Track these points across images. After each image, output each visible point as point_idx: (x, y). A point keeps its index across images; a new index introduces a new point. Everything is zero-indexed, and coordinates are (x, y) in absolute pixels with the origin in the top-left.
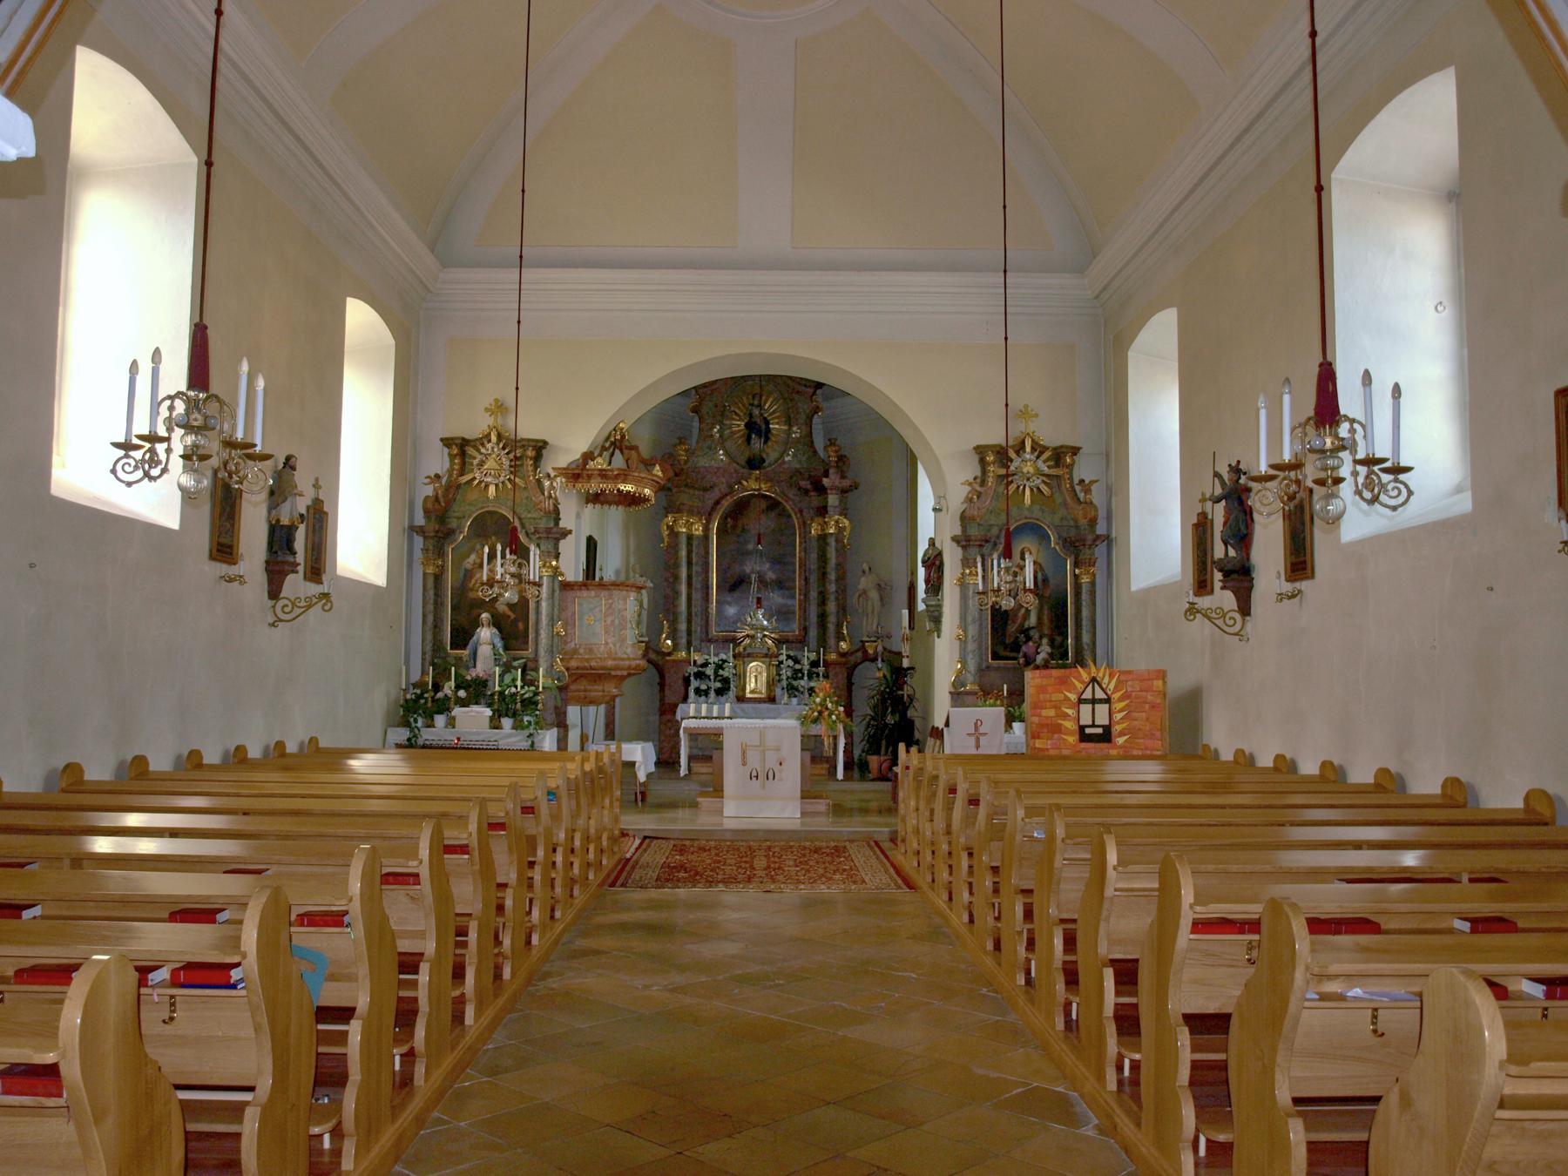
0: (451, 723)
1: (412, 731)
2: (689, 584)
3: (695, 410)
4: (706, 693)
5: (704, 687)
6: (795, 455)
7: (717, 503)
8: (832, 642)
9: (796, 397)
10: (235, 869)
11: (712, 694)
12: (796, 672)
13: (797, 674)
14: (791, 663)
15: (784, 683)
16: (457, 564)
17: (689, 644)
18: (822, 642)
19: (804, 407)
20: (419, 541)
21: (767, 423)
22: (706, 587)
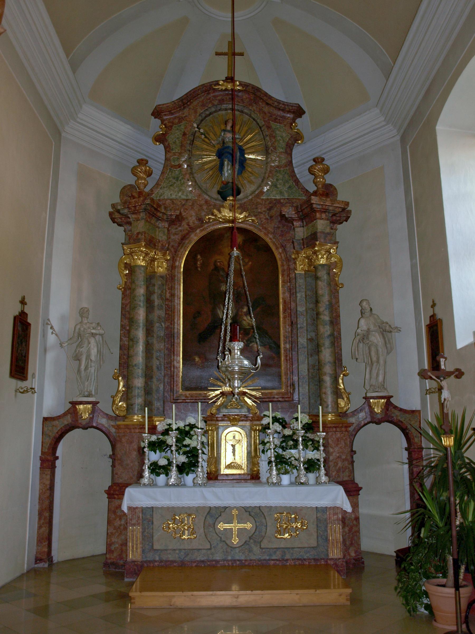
2: (149, 331)
3: (160, 139)
4: (166, 470)
5: (163, 462)
6: (274, 185)
7: (184, 238)
8: (329, 399)
9: (273, 125)
11: (174, 472)
12: (286, 438)
13: (289, 441)
14: (277, 427)
15: (271, 454)
17: (148, 403)
18: (317, 397)
19: (282, 134)
21: (242, 152)
22: (170, 336)
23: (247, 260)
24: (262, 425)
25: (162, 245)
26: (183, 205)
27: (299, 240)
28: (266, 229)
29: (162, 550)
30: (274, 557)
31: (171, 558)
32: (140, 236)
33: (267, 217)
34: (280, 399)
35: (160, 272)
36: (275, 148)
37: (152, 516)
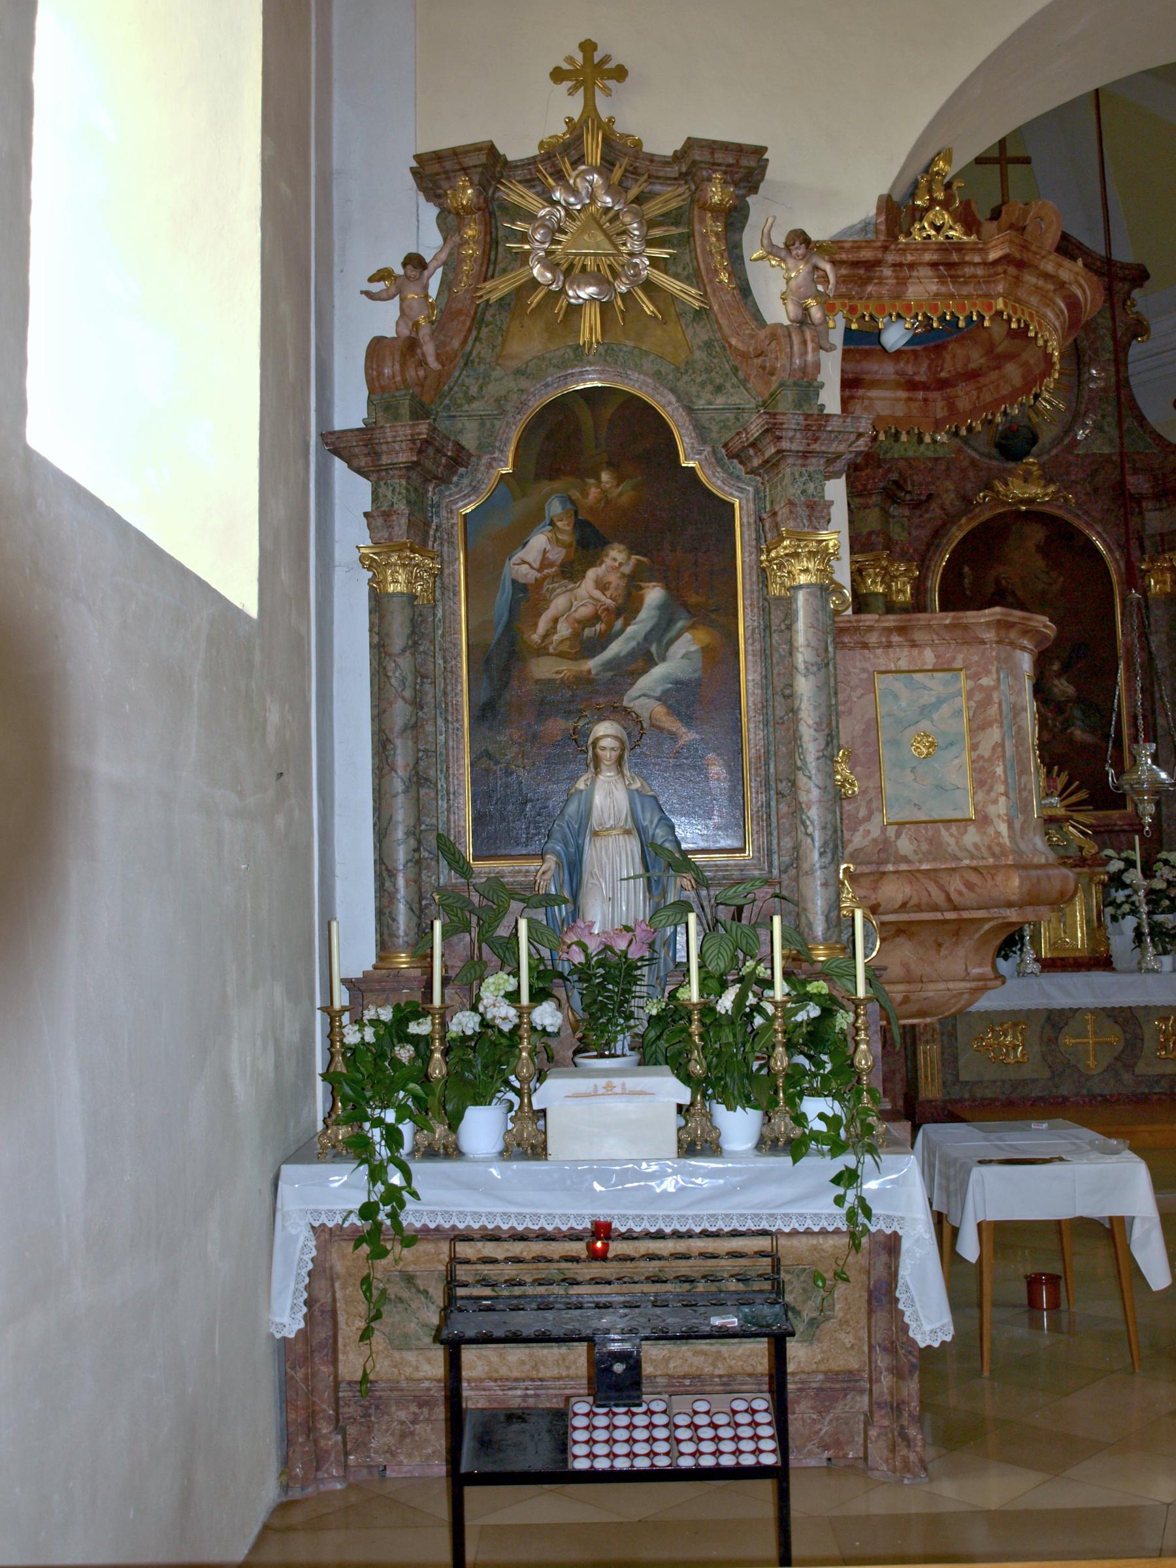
0: (528, 1143)
1: (377, 1174)
6: (1098, 428)
7: (938, 534)
10: (503, 184)
16: (483, 572)
20: (353, 492)
23: (1054, 574)
24: (1108, 873)
25: (902, 549)
26: (931, 470)
27: (1153, 536)
28: (1086, 512)
29: (975, 1083)
30: (1157, 1090)
31: (989, 1094)
32: (874, 537)
33: (1088, 489)
34: (1126, 827)
35: (901, 603)
36: (1096, 352)
37: (954, 1026)
